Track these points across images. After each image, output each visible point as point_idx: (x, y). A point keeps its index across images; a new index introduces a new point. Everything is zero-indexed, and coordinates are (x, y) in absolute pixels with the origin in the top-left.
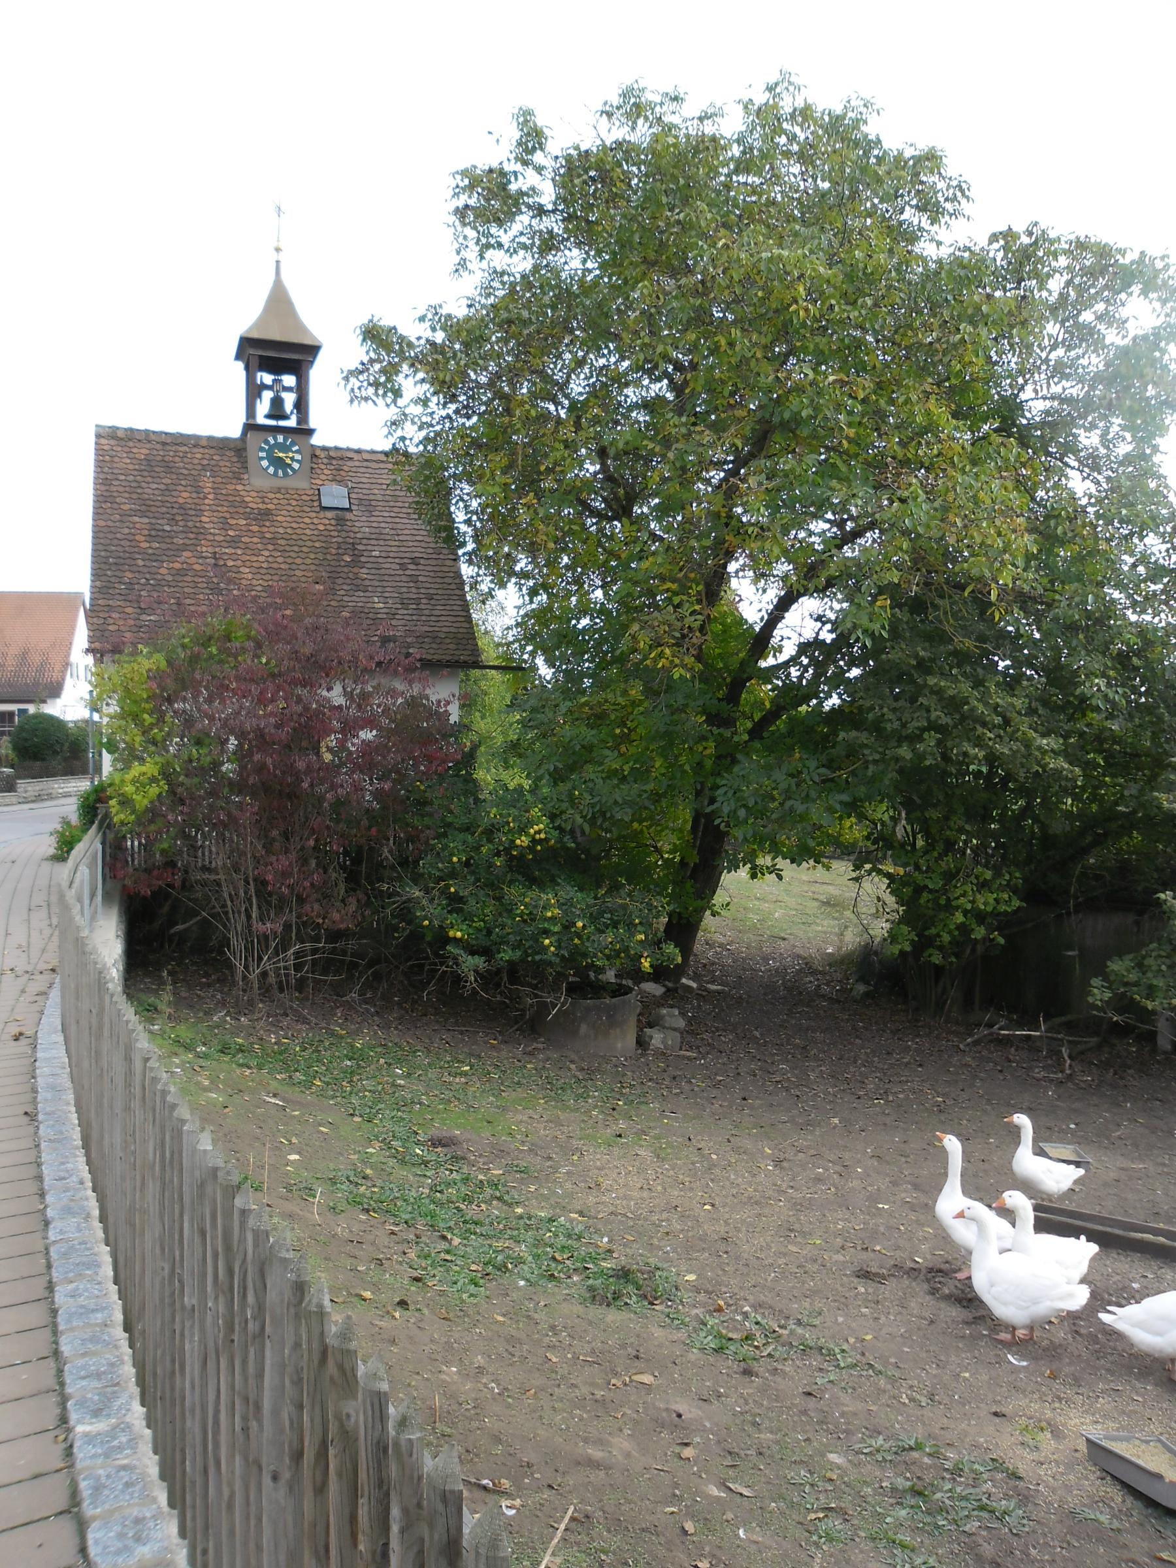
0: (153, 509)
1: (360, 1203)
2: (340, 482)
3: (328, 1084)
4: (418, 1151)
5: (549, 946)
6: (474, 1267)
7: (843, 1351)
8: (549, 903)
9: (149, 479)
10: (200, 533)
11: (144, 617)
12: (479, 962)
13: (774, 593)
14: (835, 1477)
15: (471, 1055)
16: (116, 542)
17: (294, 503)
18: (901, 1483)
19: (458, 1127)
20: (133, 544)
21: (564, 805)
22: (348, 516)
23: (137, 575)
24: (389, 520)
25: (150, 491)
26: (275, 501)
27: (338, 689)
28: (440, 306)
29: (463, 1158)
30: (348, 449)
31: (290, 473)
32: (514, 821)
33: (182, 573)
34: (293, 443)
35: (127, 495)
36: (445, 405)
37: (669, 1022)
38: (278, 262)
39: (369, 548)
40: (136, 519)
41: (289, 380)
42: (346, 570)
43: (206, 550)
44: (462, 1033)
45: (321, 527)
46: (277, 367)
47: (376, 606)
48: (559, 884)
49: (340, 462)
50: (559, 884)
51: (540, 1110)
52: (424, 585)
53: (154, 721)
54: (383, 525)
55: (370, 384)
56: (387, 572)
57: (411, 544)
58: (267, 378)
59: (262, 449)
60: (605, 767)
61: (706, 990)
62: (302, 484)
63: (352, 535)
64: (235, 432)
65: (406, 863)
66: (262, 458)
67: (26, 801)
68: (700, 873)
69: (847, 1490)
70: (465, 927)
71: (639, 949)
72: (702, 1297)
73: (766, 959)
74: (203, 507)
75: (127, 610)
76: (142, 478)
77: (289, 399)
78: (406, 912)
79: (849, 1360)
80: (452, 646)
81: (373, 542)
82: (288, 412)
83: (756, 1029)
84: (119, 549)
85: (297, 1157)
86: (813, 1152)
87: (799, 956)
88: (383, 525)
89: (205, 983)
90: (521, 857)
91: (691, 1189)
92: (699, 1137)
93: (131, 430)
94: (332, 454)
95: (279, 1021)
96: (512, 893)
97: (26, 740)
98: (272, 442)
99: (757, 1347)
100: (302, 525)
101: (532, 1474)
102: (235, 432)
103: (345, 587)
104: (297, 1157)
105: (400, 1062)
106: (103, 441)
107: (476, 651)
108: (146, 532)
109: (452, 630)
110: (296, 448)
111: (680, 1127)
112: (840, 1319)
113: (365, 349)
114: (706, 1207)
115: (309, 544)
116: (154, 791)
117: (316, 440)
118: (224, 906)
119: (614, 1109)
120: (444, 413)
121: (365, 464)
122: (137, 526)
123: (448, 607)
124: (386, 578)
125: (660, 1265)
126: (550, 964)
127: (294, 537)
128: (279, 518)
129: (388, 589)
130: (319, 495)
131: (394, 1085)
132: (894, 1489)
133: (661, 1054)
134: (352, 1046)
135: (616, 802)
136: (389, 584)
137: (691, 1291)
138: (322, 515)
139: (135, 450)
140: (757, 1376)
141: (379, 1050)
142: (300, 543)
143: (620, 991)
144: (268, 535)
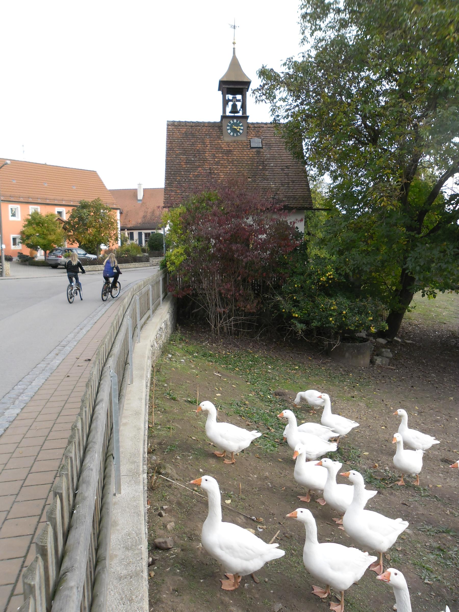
0: (188, 152)
1: (238, 413)
2: (258, 137)
3: (241, 370)
4: (269, 397)
5: (332, 321)
6: (276, 440)
7: (425, 489)
8: (334, 304)
9: (186, 141)
10: (205, 160)
11: (184, 194)
12: (303, 326)
13: (444, 172)
14: (405, 538)
15: (300, 362)
16: (174, 166)
17: (240, 146)
18: (435, 545)
19: (288, 389)
20: (180, 166)
21: (342, 265)
22: (262, 150)
23: (181, 178)
24: (277, 151)
25: (186, 145)
26: (233, 146)
27: (250, 218)
28: (292, 58)
29: (286, 401)
30: (262, 123)
31: (239, 134)
32: (320, 271)
33: (198, 176)
34: (240, 123)
35: (178, 147)
36: (296, 101)
37: (385, 354)
38: (234, 48)
39: (269, 163)
40: (181, 156)
41: (239, 97)
42: (260, 172)
43: (207, 167)
44: (298, 354)
45: (251, 155)
46: (234, 92)
47: (271, 186)
48: (338, 296)
49: (259, 129)
50: (338, 296)
51: (323, 385)
52: (291, 177)
53: (182, 232)
54: (275, 153)
55: (263, 94)
56: (276, 172)
57: (286, 160)
58: (230, 97)
59: (228, 126)
60: (360, 249)
61: (406, 343)
62: (243, 138)
63: (263, 158)
64: (218, 120)
65: (277, 287)
66: (228, 129)
67: (153, 265)
68: (404, 296)
69: (409, 543)
70: (299, 313)
71: (370, 323)
72: (369, 462)
73: (435, 331)
74: (206, 150)
75: (178, 191)
76: (185, 140)
77: (239, 104)
78: (276, 306)
79: (427, 493)
80: (301, 201)
81: (271, 160)
82: (239, 110)
83: (424, 359)
84: (175, 168)
85: (220, 395)
86: (437, 410)
87: (450, 331)
88: (275, 153)
89: (203, 331)
90: (323, 285)
91: (378, 420)
92: (387, 400)
93: (180, 122)
94: (255, 126)
95: (227, 346)
96: (318, 299)
97: (153, 243)
98: (232, 122)
99: (387, 483)
100: (243, 155)
101: (273, 518)
102: (218, 120)
103: (260, 179)
104: (220, 395)
105: (271, 364)
106: (170, 127)
107: (311, 203)
108: (185, 161)
109: (302, 195)
110: (241, 124)
111: (380, 396)
112: (428, 477)
113: (260, 80)
114: (383, 427)
115: (246, 162)
116: (182, 258)
117: (250, 121)
118: (208, 303)
119: (354, 387)
120: (295, 104)
121: (268, 129)
122: (182, 159)
123: (300, 186)
124: (276, 174)
125: (355, 447)
126: (333, 328)
127: (240, 160)
128: (234, 153)
129: (276, 179)
130: (250, 142)
131: (267, 372)
132: (431, 547)
133: (380, 367)
134: (254, 357)
135: (364, 263)
136: (277, 177)
137: (365, 459)
138: (251, 151)
139: (181, 130)
140: (383, 494)
141: (264, 359)
142: (242, 162)
143: (364, 340)
144: (230, 160)
